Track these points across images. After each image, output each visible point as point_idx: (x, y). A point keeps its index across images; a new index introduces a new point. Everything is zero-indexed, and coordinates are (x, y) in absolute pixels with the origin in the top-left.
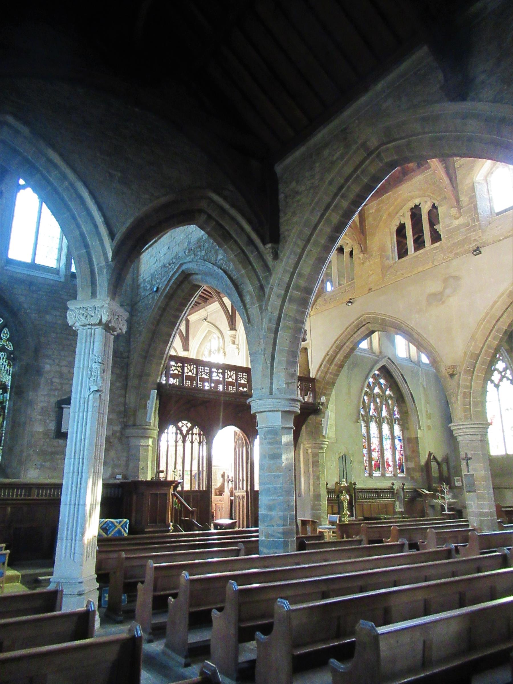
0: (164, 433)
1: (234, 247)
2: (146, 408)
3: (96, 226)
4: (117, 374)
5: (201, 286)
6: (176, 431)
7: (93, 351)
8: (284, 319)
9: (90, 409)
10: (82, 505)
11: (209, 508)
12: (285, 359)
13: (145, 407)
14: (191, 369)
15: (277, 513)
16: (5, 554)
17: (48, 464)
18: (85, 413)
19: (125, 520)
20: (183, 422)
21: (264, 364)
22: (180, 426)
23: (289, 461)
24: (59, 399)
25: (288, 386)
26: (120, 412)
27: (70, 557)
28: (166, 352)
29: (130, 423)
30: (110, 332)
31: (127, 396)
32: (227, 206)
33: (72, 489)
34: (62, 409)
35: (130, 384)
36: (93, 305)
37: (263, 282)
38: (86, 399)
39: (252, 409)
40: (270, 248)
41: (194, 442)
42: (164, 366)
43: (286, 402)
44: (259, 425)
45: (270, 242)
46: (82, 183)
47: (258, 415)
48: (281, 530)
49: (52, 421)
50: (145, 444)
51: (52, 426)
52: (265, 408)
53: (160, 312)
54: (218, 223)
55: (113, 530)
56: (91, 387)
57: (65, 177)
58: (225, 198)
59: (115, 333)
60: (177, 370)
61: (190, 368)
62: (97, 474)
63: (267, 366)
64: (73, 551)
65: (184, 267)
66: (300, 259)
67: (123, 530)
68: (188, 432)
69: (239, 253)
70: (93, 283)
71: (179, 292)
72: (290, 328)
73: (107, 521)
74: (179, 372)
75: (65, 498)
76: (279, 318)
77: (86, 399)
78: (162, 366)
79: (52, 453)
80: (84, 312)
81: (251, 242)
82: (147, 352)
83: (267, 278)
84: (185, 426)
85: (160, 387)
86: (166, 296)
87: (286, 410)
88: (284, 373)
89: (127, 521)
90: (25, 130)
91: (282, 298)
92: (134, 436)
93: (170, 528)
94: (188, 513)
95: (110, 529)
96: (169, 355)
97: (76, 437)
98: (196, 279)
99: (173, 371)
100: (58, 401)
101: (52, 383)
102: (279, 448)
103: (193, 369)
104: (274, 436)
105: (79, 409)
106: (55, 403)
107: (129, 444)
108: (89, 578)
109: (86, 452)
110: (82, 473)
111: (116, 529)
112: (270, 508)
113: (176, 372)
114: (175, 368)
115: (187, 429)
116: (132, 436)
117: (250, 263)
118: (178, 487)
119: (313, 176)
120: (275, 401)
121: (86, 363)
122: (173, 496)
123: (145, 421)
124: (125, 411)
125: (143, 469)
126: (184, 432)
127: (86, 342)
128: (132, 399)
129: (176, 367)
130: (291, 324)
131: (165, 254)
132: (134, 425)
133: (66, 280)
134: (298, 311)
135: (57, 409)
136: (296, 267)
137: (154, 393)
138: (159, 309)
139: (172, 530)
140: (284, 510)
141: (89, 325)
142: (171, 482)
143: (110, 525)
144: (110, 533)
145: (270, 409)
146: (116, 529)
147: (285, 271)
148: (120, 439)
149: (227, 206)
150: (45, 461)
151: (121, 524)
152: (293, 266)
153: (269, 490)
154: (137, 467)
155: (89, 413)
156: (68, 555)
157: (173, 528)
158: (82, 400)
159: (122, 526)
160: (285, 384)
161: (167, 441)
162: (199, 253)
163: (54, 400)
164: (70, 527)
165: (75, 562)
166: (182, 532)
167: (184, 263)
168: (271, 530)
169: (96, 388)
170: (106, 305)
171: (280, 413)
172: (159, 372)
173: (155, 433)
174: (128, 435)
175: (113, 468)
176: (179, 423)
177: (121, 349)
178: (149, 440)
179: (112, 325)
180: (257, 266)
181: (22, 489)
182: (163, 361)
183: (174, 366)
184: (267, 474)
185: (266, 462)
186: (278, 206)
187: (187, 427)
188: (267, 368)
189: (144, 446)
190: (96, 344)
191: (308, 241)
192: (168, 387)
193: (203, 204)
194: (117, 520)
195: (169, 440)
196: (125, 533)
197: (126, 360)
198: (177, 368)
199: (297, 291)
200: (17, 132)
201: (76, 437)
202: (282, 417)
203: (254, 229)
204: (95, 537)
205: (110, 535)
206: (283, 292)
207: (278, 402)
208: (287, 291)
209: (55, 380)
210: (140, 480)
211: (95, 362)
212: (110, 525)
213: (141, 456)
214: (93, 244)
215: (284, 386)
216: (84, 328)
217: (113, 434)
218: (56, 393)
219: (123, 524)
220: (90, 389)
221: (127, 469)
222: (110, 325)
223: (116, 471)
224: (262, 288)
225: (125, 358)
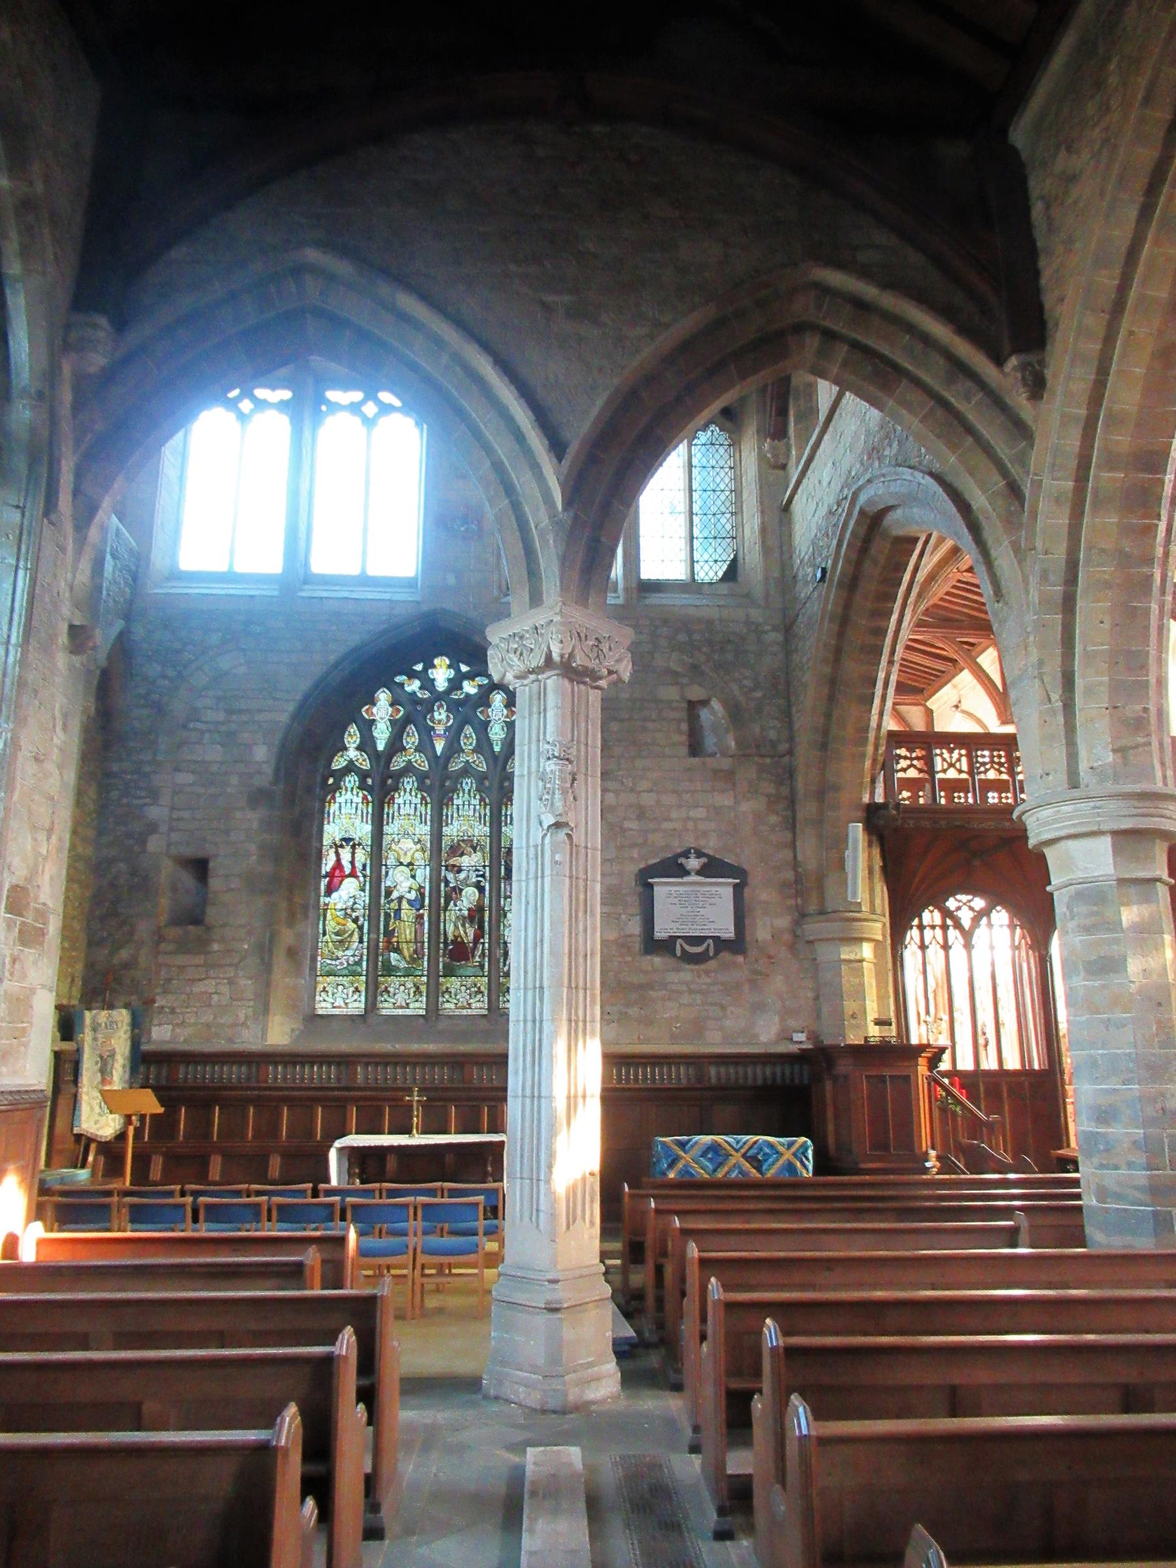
0: (911, 928)
1: (915, 396)
2: (844, 869)
3: (520, 437)
4: (768, 796)
5: (916, 540)
6: (1011, 921)
7: (545, 733)
8: (1088, 561)
9: (547, 872)
10: (546, 1098)
11: (1059, 1116)
12: (1105, 679)
13: (841, 864)
14: (953, 761)
15: (1123, 1132)
16: (477, 1204)
17: (634, 1011)
18: (540, 880)
19: (804, 1139)
20: (958, 897)
21: (1042, 703)
22: (952, 908)
23: (1155, 977)
24: (642, 866)
25: (1125, 758)
26: (785, 885)
27: (531, 1219)
28: (873, 723)
29: (812, 908)
30: (585, 683)
31: (798, 843)
32: (869, 291)
33: (524, 1061)
34: (651, 886)
35: (800, 816)
36: (532, 625)
37: (1014, 470)
38: (539, 848)
39: (1030, 834)
40: (1014, 369)
41: (950, 947)
42: (874, 760)
43: (1121, 803)
44: (1055, 880)
45: (1016, 350)
46: (476, 346)
47: (1049, 853)
48: (1143, 1182)
49: (632, 915)
50: (852, 957)
51: (635, 927)
52: (1057, 829)
53: (835, 628)
54: (855, 345)
55: (773, 1163)
56: (543, 817)
57: (439, 343)
58: (864, 273)
59: (603, 683)
60: (914, 766)
61: (951, 757)
62: (581, 1024)
63: (1052, 708)
64: (535, 1207)
65: (862, 499)
66: (1103, 371)
67: (798, 1164)
68: (976, 921)
69: (932, 409)
70: (533, 573)
71: (867, 566)
72: (1108, 585)
73: (757, 1141)
74: (920, 771)
75: (515, 1082)
76: (1072, 566)
77: (539, 848)
78: (868, 764)
79: (641, 987)
80: (516, 646)
81: (960, 368)
82: (826, 732)
83: (1022, 460)
84: (965, 908)
85: (873, 816)
86: (840, 584)
87: (1123, 827)
88: (1106, 721)
89: (806, 1142)
90: (343, 268)
91: (1069, 505)
92: (822, 940)
93: (928, 1165)
94: (975, 1127)
95: (766, 1160)
96: (883, 731)
97: (526, 937)
98: (897, 522)
99: (904, 770)
100: (641, 871)
101: (623, 830)
102: (1116, 941)
103: (959, 760)
104: (1096, 908)
105: (527, 874)
106: (636, 875)
107: (815, 959)
108: (577, 1273)
109: (545, 971)
110: (541, 1021)
111: (781, 1162)
112: (1104, 1115)
113: (912, 773)
114: (908, 762)
115: (971, 914)
116: (822, 940)
117: (970, 430)
118: (940, 1060)
119: (1105, 109)
120: (1085, 806)
121: (534, 763)
122: (929, 1084)
123: (846, 899)
124: (798, 880)
125: (853, 1016)
126: (966, 923)
127: (530, 715)
128: (808, 850)
129: (911, 759)
130: (1108, 571)
131: (830, 483)
132: (822, 912)
133: (628, 599)
134: (1125, 530)
135: (640, 889)
136: (1096, 400)
137: (857, 830)
138: (831, 620)
139: (935, 1170)
140: (1148, 1123)
141: (531, 673)
142: (922, 1048)
143: (767, 1150)
144: (768, 1170)
145: (1072, 831)
146: (781, 1162)
147: (1066, 420)
148: (792, 948)
149: (869, 291)
150: (629, 1004)
151: (793, 1149)
152: (1085, 399)
153: (1094, 1063)
154: (839, 1014)
155: (547, 880)
156: (527, 1214)
157: (938, 1164)
158: (532, 850)
159: (794, 1154)
160: (1114, 751)
161: (992, 947)
162: (887, 452)
163: (633, 868)
164: (526, 1148)
165: (540, 1231)
166: (964, 1173)
167: (860, 489)
168: (1110, 1178)
169: (552, 821)
170: (557, 618)
171: (1107, 841)
172: (862, 776)
173: (878, 928)
174: (812, 938)
175: (782, 1020)
176: (947, 900)
177: (772, 735)
178: (861, 946)
179: (579, 662)
180: (990, 430)
181: (329, 1064)
182: (870, 749)
183: (905, 758)
184: (1084, 1018)
185: (1079, 981)
186: (1032, 243)
187: (971, 909)
188: (1053, 712)
189: (850, 961)
190: (550, 714)
191: (1118, 307)
192: (894, 812)
193: (802, 307)
194: (782, 1140)
195: (989, 951)
196: (804, 1171)
197: (786, 759)
198: (915, 762)
199: (1112, 469)
200: (331, 278)
201: (526, 937)
202: (1117, 850)
203: (963, 330)
204: (592, 1174)
205: (769, 1175)
206: (1070, 484)
207: (1095, 807)
208: (1081, 477)
209: (627, 824)
210: (849, 1042)
211: (549, 759)
212: (767, 1150)
213: (846, 987)
214: (524, 482)
215: (1110, 757)
216: (525, 682)
217: (773, 936)
218: (635, 853)
219: (798, 1150)
220: (541, 824)
221: (818, 1017)
222: (574, 665)
223: (792, 1023)
224: (1014, 490)
225: (784, 755)
